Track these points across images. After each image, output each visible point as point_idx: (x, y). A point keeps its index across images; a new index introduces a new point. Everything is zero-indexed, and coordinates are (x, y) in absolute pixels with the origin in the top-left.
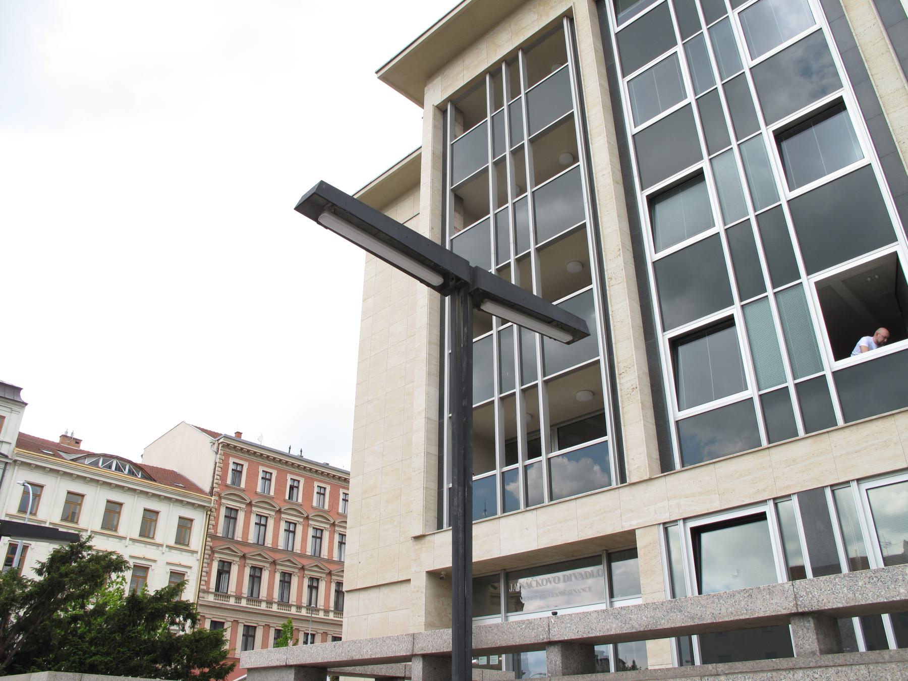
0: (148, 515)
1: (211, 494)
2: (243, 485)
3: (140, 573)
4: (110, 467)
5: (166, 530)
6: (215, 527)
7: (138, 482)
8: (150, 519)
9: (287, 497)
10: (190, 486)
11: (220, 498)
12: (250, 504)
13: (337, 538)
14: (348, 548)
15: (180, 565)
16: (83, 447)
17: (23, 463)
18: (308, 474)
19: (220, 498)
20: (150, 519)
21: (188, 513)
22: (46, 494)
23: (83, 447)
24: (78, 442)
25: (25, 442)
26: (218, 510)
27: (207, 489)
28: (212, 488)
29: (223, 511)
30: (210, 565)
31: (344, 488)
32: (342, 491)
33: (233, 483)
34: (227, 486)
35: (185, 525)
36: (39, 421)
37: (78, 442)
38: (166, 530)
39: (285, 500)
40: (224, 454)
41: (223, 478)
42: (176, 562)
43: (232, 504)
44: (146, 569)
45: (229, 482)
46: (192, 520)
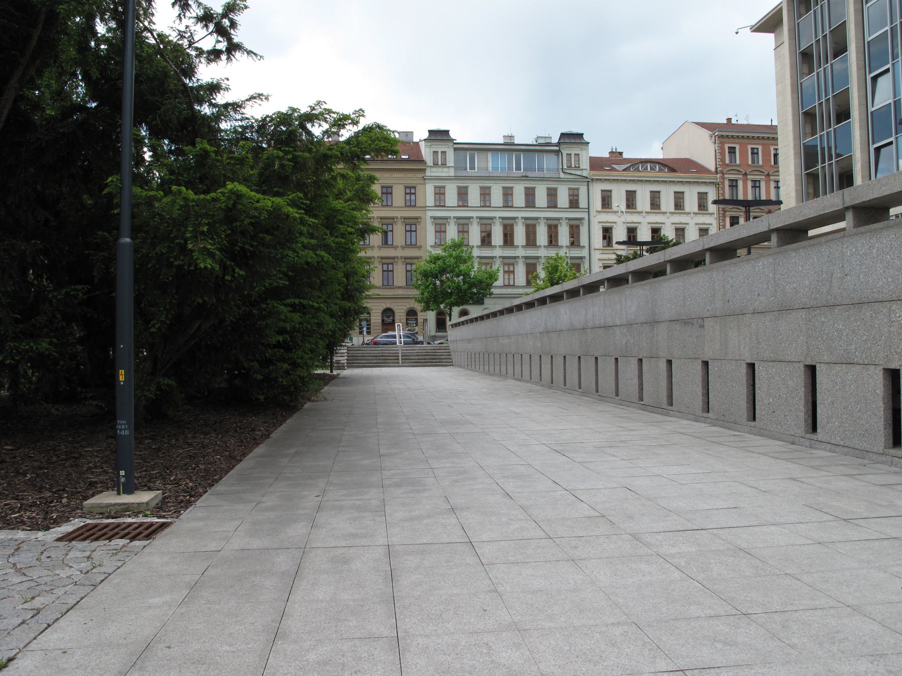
0: (605, 193)
1: (716, 172)
2: (738, 162)
3: (680, 233)
4: (646, 168)
5: (691, 203)
6: (723, 194)
7: (666, 175)
8: (631, 198)
9: (773, 163)
10: (702, 169)
11: (723, 174)
12: (745, 174)
13: (772, 185)
14: (782, 190)
15: (607, 222)
16: (625, 156)
17: (597, 180)
18: (763, 142)
19: (723, 174)
20: (631, 198)
21: (703, 189)
22: (687, 197)
23: (625, 156)
24: (621, 154)
25: (596, 164)
26: (723, 183)
27: (713, 169)
28: (716, 168)
29: (727, 183)
30: (724, 220)
31: (773, 145)
32: (772, 148)
33: (731, 161)
34: (727, 165)
35: (702, 197)
36: (599, 149)
37: (621, 154)
38: (691, 203)
39: (771, 166)
40: (721, 143)
41: (723, 160)
42: (654, 221)
43: (757, 178)
44: (683, 230)
45: (727, 161)
46: (611, 191)
